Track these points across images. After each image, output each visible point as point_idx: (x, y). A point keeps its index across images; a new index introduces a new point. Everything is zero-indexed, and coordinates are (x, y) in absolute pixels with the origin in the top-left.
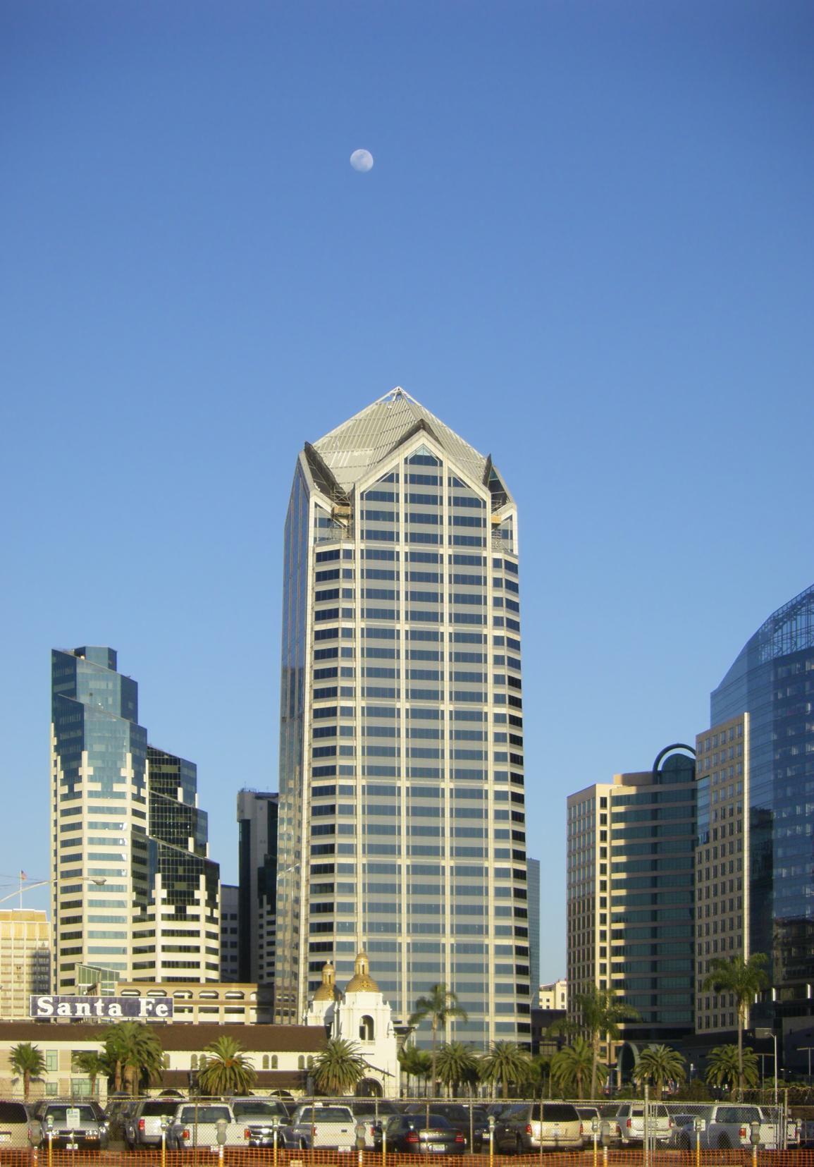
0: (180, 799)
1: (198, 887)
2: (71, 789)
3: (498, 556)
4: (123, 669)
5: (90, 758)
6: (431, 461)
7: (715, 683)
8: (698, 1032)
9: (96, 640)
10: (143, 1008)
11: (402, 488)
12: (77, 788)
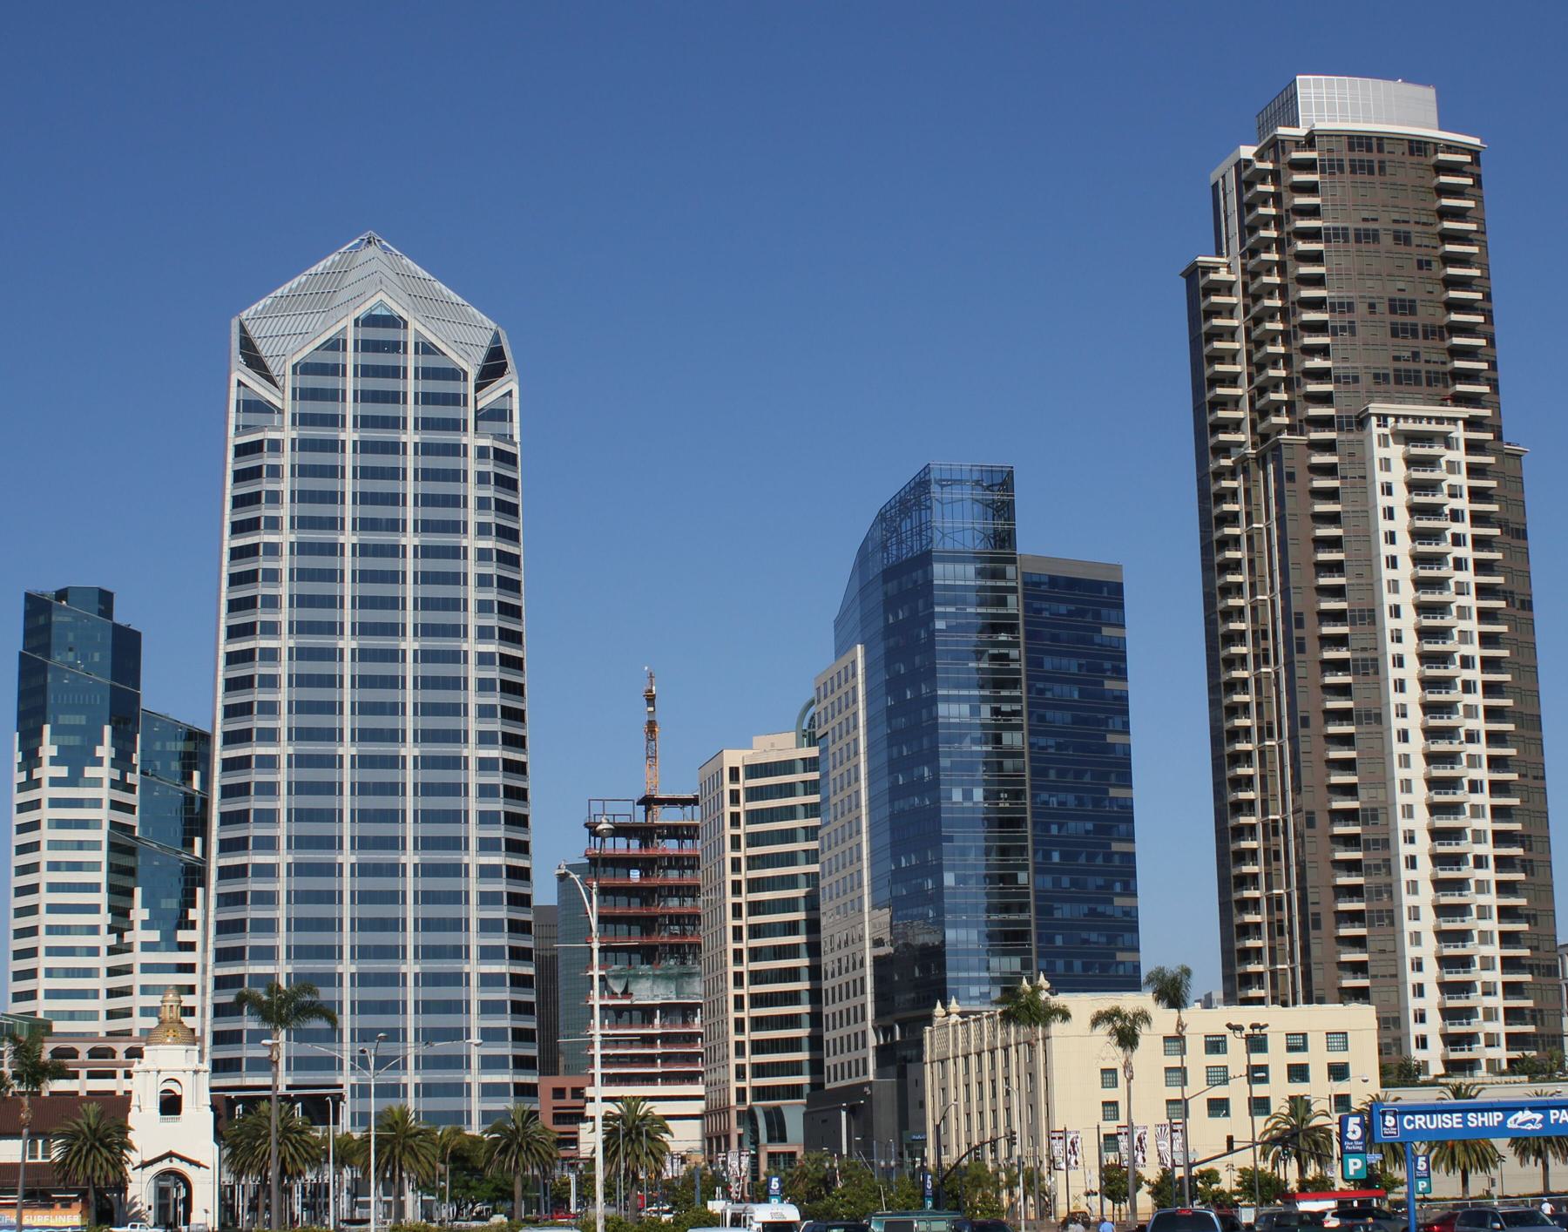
2: (30, 775)
4: (120, 617)
5: (53, 733)
6: (392, 322)
7: (835, 611)
8: (828, 1086)
12: (37, 774)
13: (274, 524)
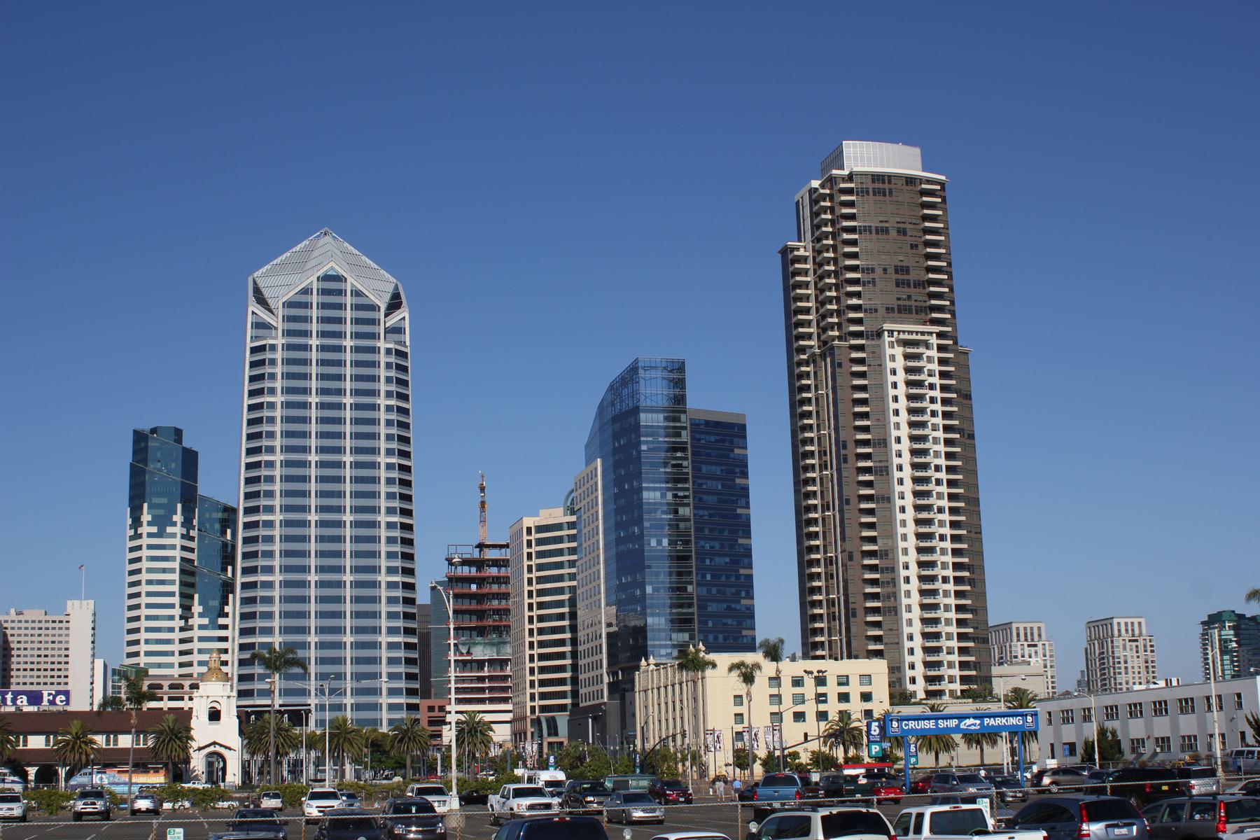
4: (187, 443)
6: (338, 278)
9: (167, 421)
10: (46, 698)
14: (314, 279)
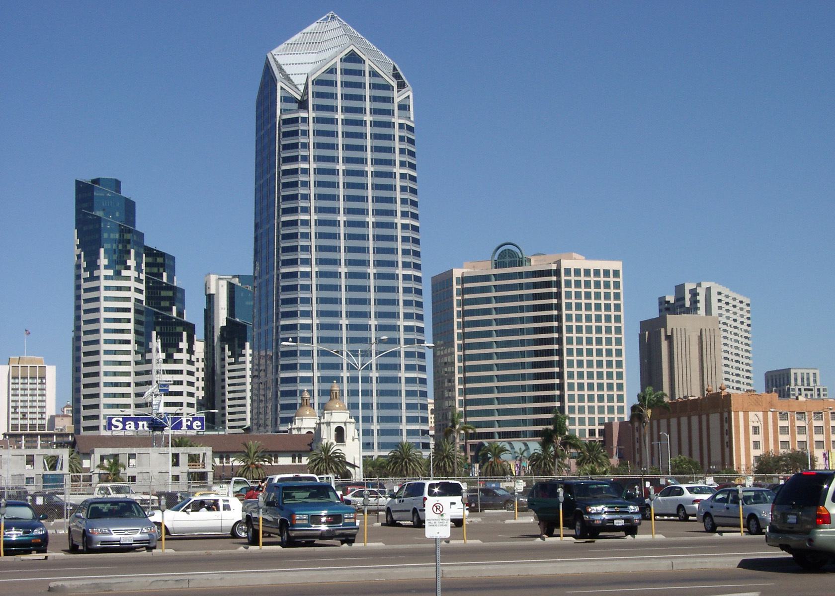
0: (165, 280)
1: (182, 341)
2: (92, 274)
3: (402, 121)
4: (124, 193)
10: (184, 424)
11: (339, 78)
12: (96, 273)
13: (305, 159)
14: (338, 60)
